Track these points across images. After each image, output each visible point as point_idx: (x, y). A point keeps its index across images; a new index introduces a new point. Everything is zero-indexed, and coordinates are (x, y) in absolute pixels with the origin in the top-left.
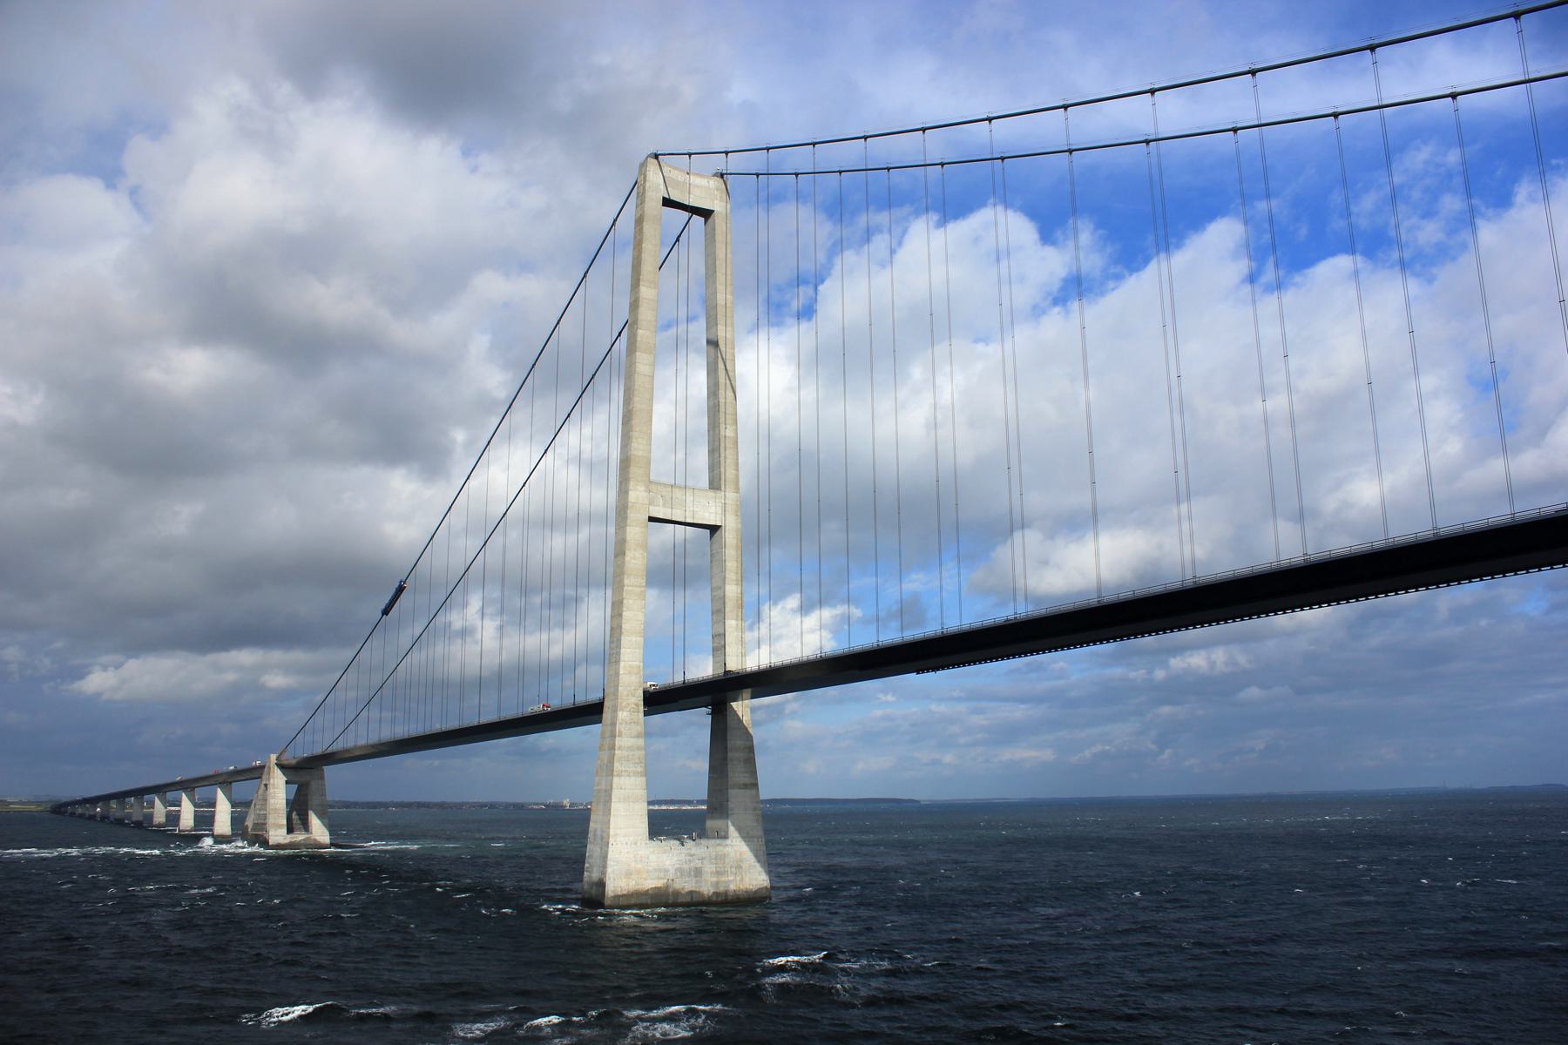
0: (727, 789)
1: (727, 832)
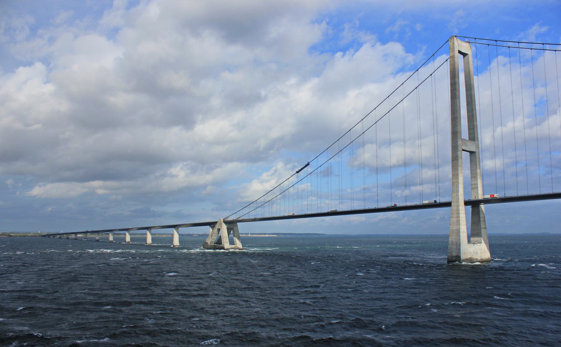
0: (481, 229)
1: (481, 241)
